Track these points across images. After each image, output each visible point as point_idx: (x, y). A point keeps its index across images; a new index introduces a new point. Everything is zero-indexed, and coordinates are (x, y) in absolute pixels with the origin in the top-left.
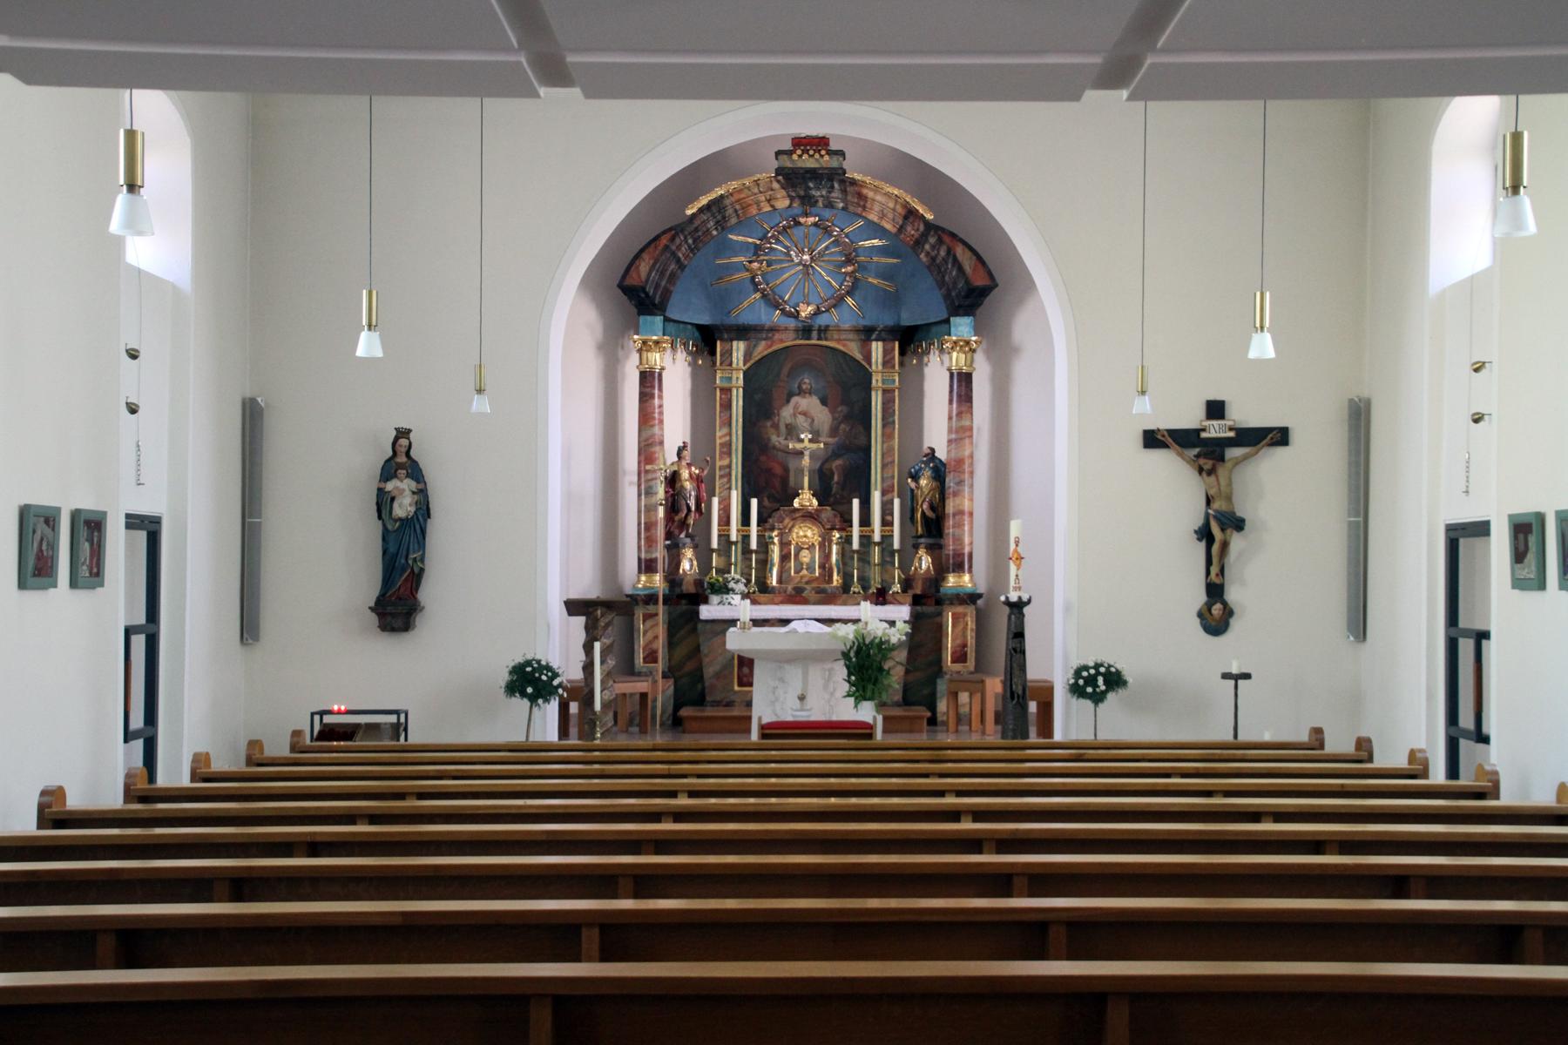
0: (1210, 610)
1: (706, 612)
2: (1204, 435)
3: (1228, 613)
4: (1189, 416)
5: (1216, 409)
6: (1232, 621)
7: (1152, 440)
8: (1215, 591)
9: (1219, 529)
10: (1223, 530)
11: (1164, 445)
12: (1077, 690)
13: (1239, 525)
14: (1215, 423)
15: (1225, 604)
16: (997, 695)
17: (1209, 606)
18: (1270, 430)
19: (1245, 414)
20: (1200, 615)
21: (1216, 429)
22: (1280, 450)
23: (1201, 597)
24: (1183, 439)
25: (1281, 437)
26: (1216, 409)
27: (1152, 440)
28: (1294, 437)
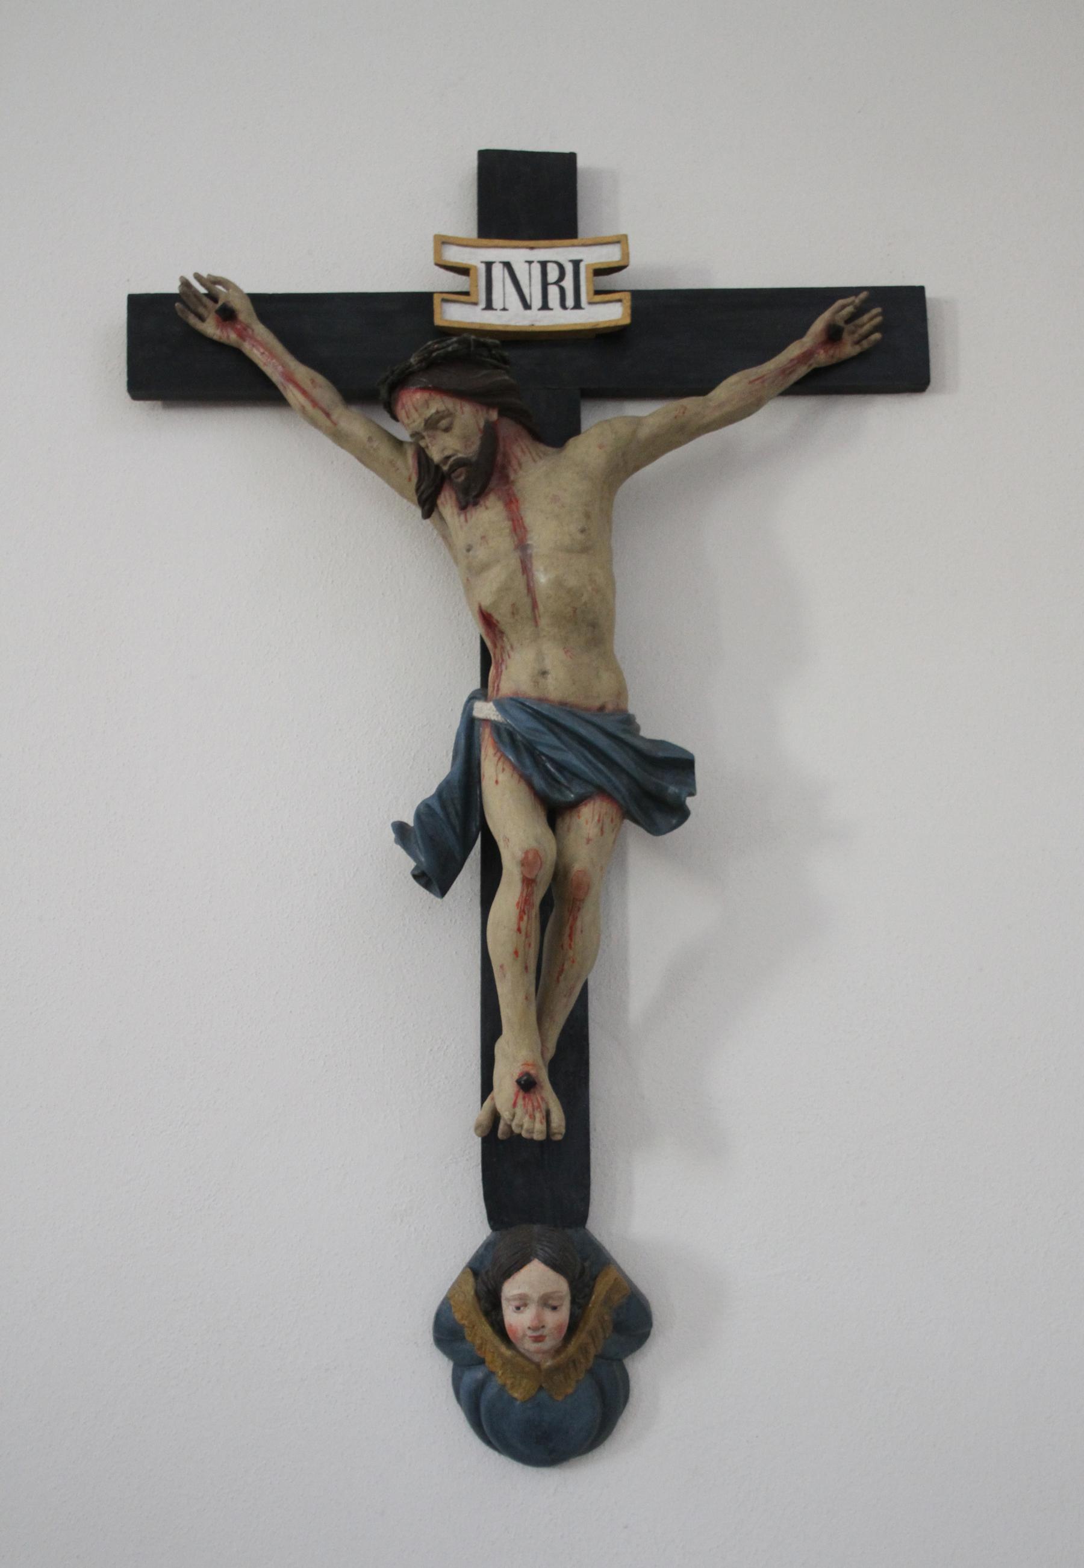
0: (490, 1303)
1: (500, 1134)
2: (454, 315)
3: (612, 1322)
4: (383, 227)
5: (527, 195)
6: (645, 1369)
7: (182, 352)
8: (537, 1185)
9: (557, 800)
10: (555, 813)
11: (251, 389)
12: (682, 406)
13: (655, 787)
14: (521, 256)
15: (584, 1265)
16: (667, 788)
17: (487, 1277)
18: (792, 306)
19: (682, 223)
20: (447, 1334)
21: (521, 293)
22: (883, 417)
23: (462, 1225)
24: (360, 351)
25: (879, 345)
26: (527, 195)
27: (182, 352)
28: (957, 340)
